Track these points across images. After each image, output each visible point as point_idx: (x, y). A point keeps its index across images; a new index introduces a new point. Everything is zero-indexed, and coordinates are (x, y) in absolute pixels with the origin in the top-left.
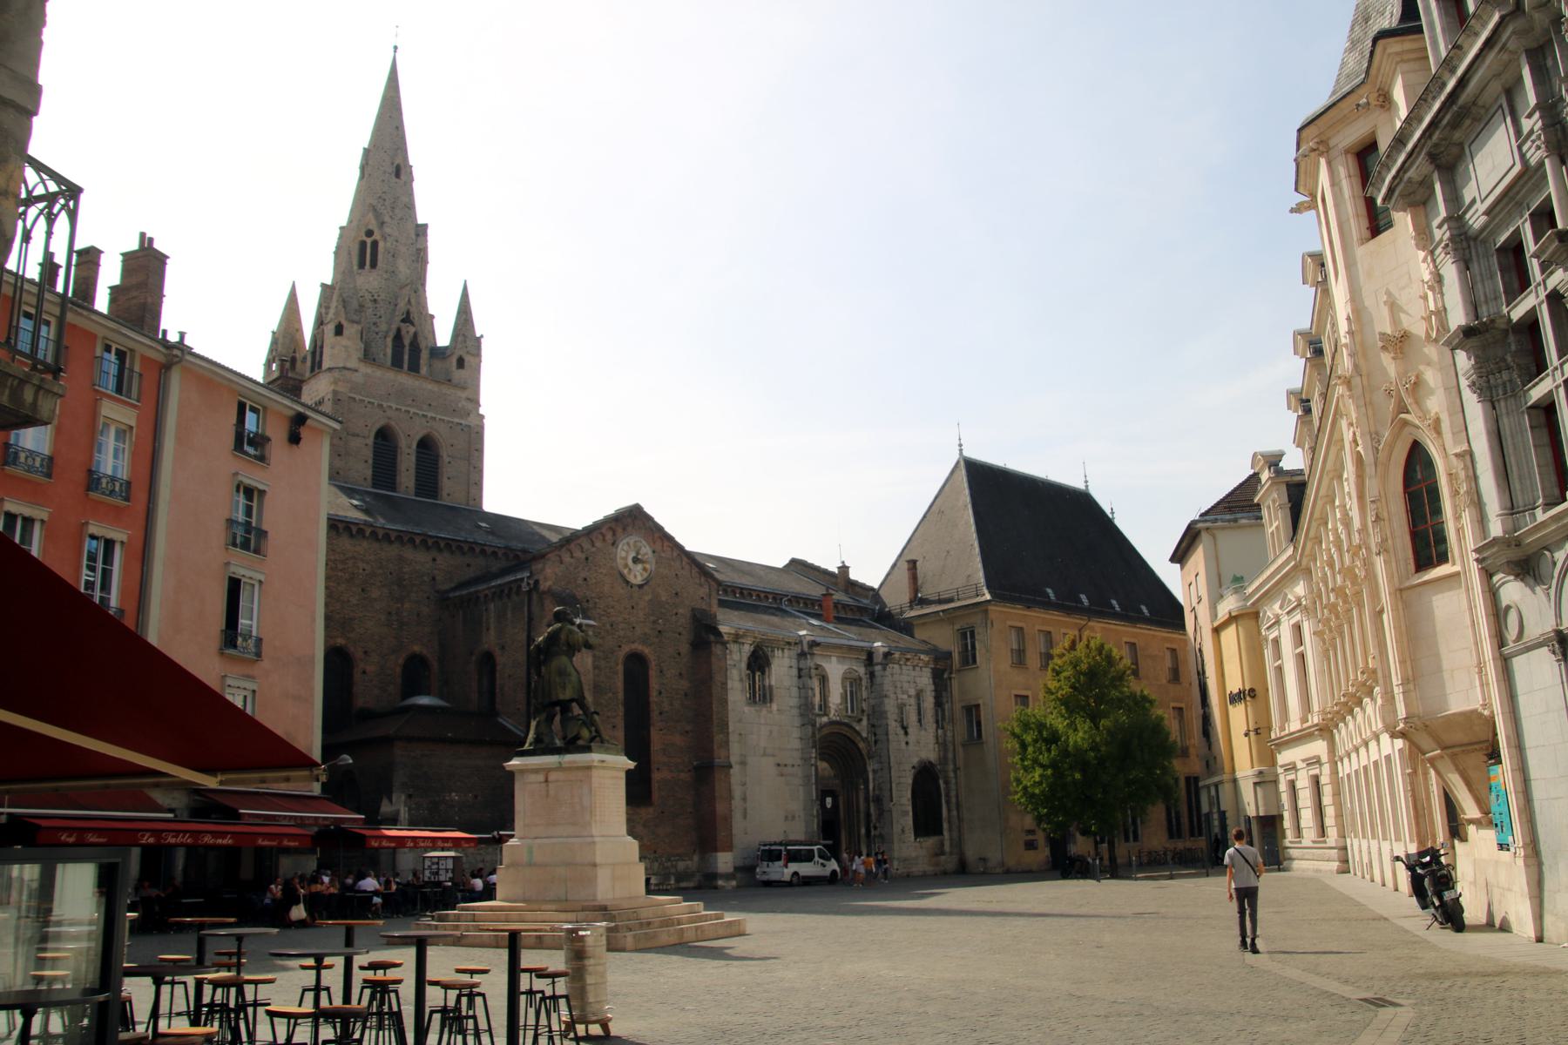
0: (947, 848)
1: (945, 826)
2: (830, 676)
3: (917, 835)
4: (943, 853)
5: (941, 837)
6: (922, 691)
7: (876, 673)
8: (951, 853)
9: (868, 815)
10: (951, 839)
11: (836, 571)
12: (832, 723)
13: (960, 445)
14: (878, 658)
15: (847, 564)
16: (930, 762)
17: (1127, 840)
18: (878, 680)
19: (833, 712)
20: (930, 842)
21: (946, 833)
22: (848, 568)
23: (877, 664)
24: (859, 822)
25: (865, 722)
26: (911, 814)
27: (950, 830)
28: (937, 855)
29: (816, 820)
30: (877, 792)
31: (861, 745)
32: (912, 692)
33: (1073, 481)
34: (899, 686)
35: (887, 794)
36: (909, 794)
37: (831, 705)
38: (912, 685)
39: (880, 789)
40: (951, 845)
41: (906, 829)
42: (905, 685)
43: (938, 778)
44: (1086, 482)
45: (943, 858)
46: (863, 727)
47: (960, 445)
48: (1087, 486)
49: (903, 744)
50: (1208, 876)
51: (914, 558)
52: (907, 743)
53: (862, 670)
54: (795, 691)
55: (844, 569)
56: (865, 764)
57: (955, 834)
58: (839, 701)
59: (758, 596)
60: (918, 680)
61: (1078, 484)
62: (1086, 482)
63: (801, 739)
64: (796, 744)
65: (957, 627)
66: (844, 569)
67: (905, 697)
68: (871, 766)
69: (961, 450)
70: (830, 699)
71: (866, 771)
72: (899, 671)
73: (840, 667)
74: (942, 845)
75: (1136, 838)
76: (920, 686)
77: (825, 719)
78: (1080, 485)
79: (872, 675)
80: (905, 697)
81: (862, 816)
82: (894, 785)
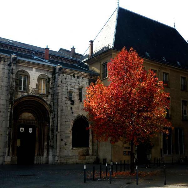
0: (90, 152)
1: (90, 143)
2: (31, 76)
3: (73, 146)
4: (88, 155)
5: (87, 148)
6: (83, 87)
7: (56, 77)
8: (93, 155)
9: (48, 136)
10: (93, 149)
11: (70, 50)
12: (29, 96)
13: (118, 3)
14: (57, 71)
15: (74, 47)
16: (84, 117)
17: (177, 153)
18: (56, 80)
19: (31, 91)
20: (81, 150)
21: (90, 147)
22: (75, 48)
23: (57, 73)
24: (44, 139)
25: (50, 97)
26: (71, 137)
27: (93, 145)
28: (84, 155)
29: (8, 136)
30: (53, 127)
31: (47, 107)
32: (77, 87)
33: (170, 24)
34: (69, 83)
35: (55, 128)
36: (70, 128)
37: (30, 88)
38: (77, 84)
39: (54, 126)
40: (93, 152)
41: (68, 144)
42: (73, 84)
43: (88, 124)
44: (175, 25)
45: (87, 157)
46: (48, 100)
47: (118, 3)
48: (175, 27)
49: (69, 108)
50: (165, 184)
51: (93, 40)
52: (71, 108)
53: (50, 76)
54: (5, 79)
55: (73, 49)
56: (49, 115)
57: (95, 147)
58: (35, 87)
59: (20, 49)
60: (80, 83)
61: (172, 26)
62: (175, 25)
63: (7, 100)
64: (4, 102)
65: (102, 63)
66: (73, 49)
67: (73, 89)
68: (51, 116)
69: (118, 4)
70: (30, 86)
71: (49, 118)
72: (69, 78)
73: (37, 73)
74: (88, 151)
75: (181, 153)
76: (81, 85)
77: (26, 94)
78: (173, 26)
79: (54, 78)
80: (73, 89)
81: (46, 137)
82: (59, 125)
